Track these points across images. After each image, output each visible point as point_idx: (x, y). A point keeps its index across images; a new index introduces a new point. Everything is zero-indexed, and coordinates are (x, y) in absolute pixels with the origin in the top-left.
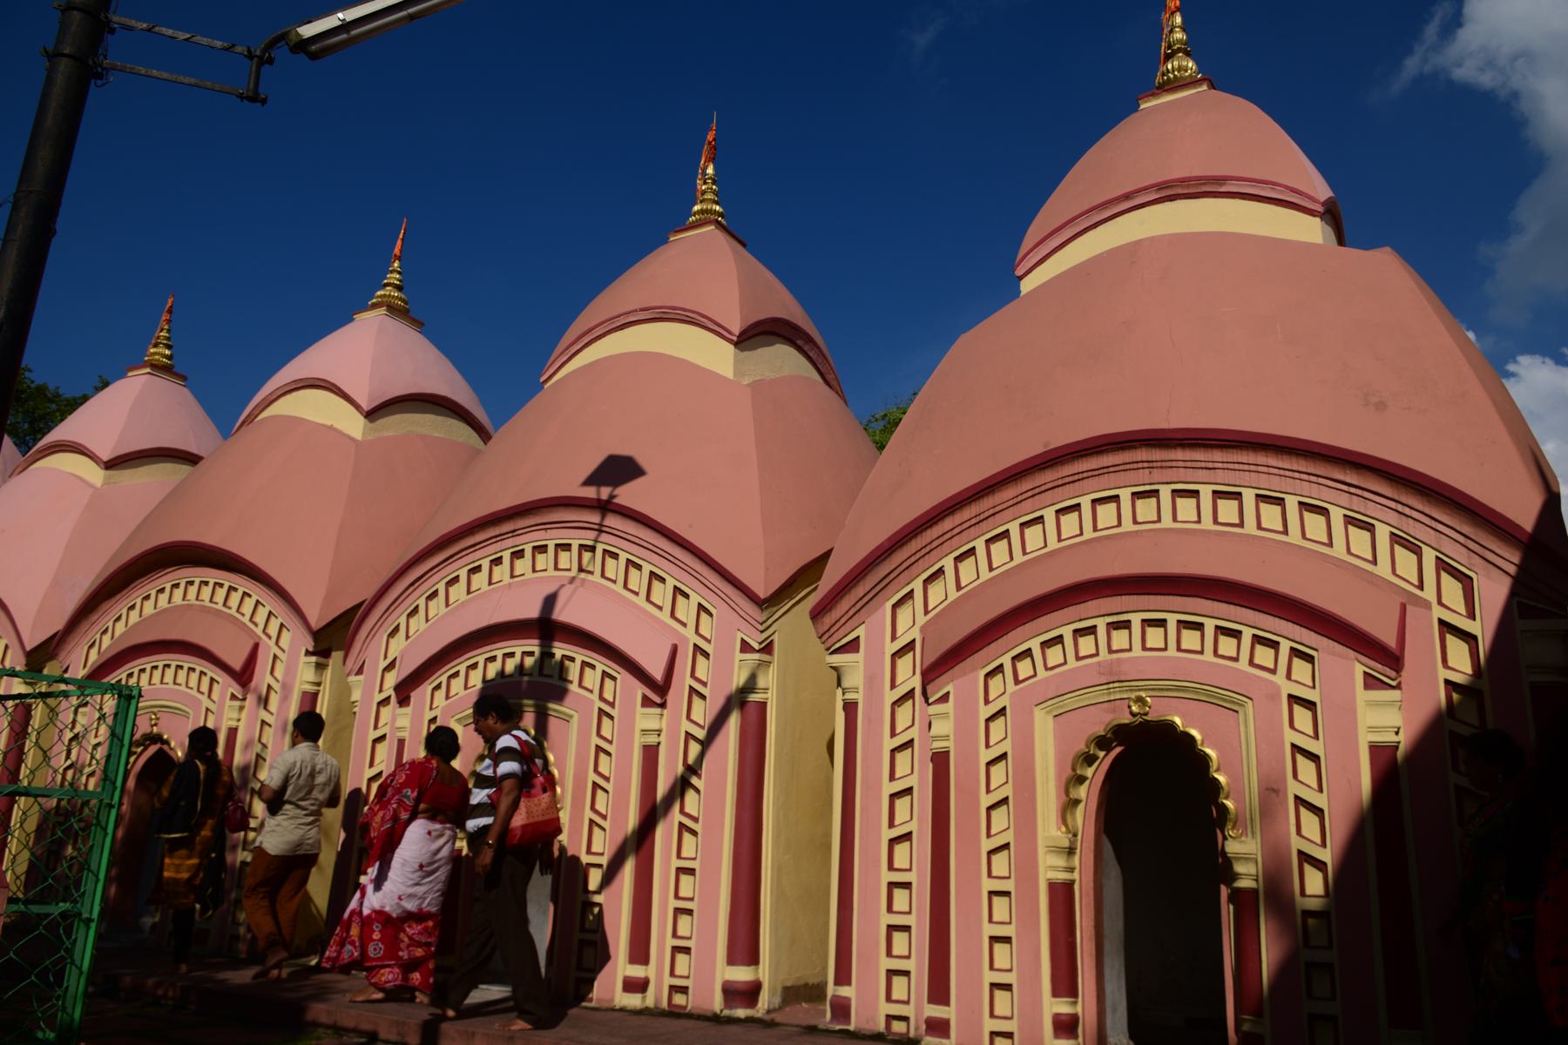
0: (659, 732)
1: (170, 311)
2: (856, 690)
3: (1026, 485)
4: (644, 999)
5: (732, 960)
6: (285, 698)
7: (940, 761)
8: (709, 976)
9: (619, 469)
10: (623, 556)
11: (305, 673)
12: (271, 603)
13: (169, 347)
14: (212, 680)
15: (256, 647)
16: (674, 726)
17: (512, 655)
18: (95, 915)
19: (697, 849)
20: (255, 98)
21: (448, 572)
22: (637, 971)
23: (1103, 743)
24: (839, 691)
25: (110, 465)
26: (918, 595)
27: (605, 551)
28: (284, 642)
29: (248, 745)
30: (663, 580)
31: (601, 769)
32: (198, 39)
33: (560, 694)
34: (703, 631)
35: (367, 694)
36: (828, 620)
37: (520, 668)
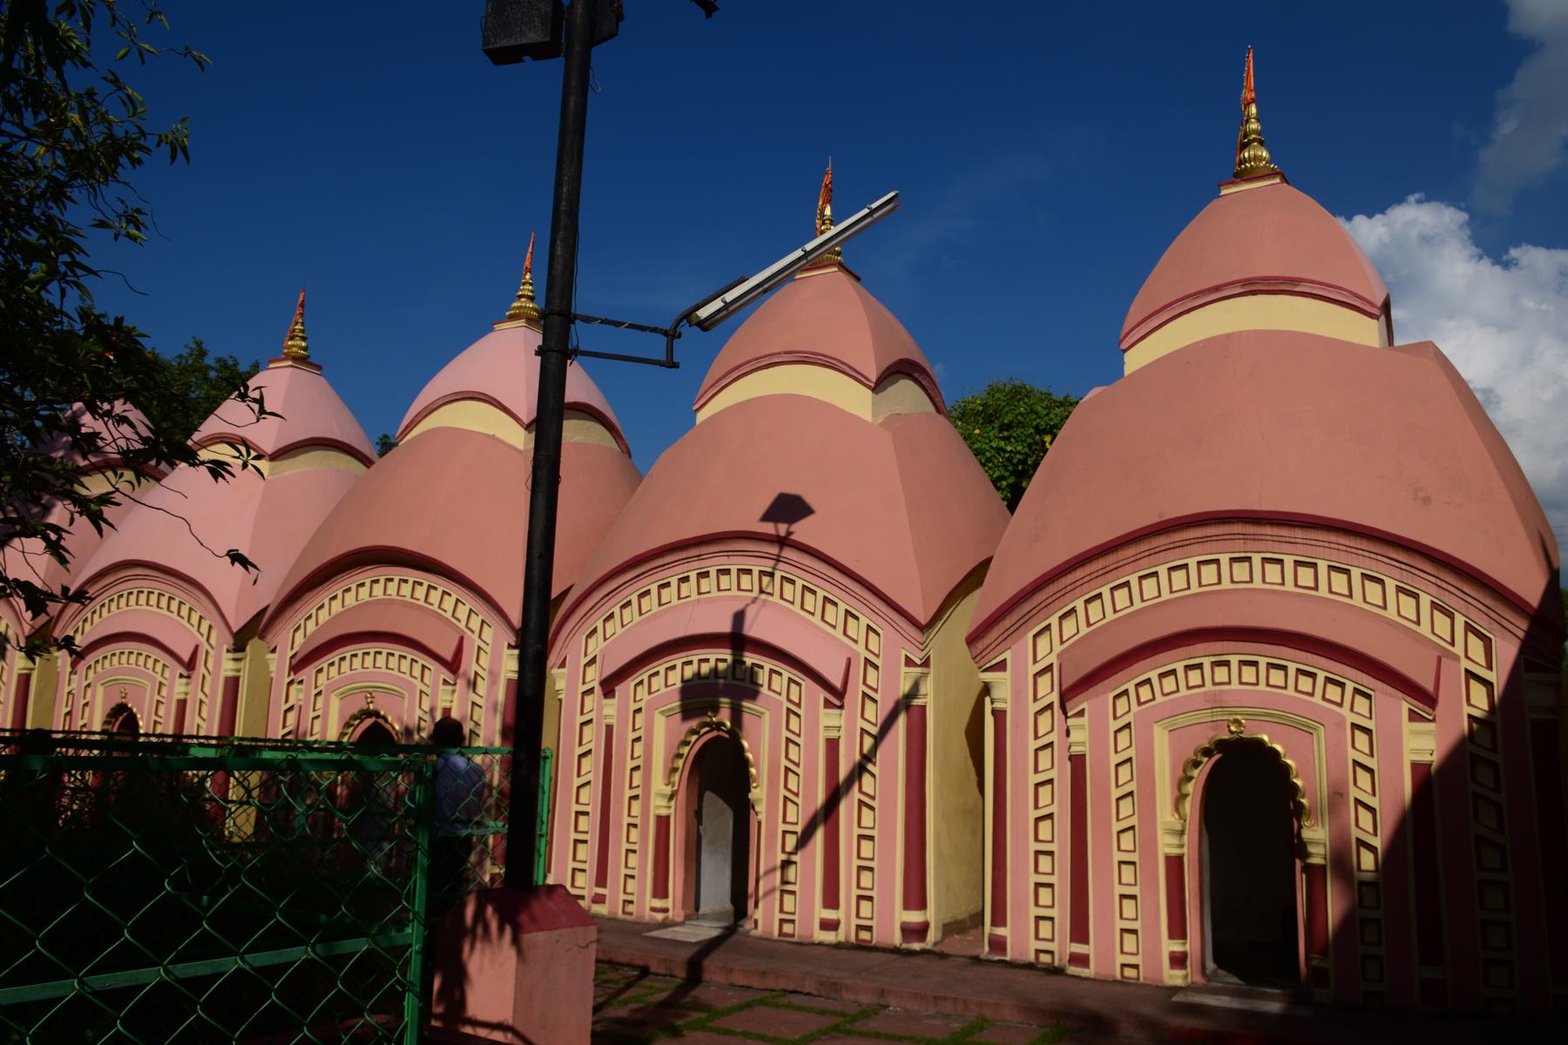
1: (302, 305)
5: (907, 907)
7: (609, 728)
8: (890, 920)
13: (304, 339)
14: (423, 667)
15: (461, 639)
16: (851, 723)
19: (874, 823)
21: (641, 586)
22: (830, 914)
26: (600, 630)
33: (753, 694)
35: (571, 685)
36: (981, 645)
37: (715, 670)
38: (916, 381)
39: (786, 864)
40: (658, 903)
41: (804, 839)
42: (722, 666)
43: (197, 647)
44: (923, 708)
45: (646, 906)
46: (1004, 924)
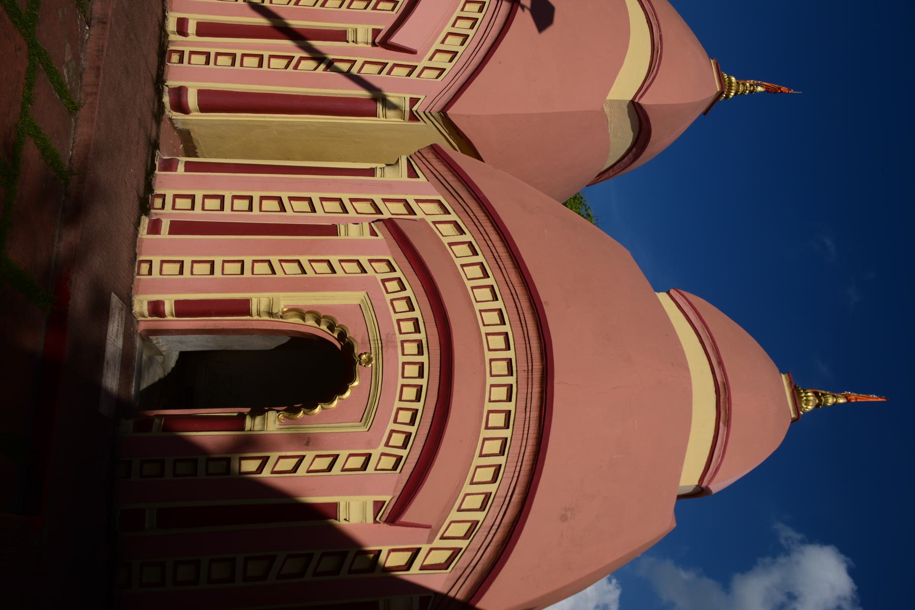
0: (355, 42)
2: (383, 175)
3: (520, 290)
4: (173, 33)
7: (332, 230)
8: (190, 77)
16: (360, 53)
22: (192, 28)
23: (342, 336)
24: (383, 165)
30: (462, 44)
34: (426, 72)
36: (430, 156)
44: (374, 114)
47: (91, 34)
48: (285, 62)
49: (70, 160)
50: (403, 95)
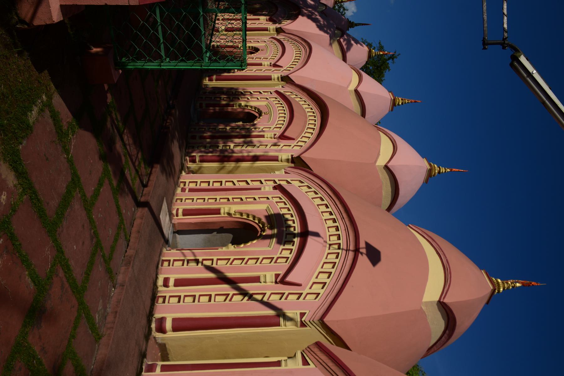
0: (265, 282)
1: (415, 102)
2: (286, 365)
4: (161, 286)
5: (174, 320)
6: (276, 151)
7: (260, 189)
8: (168, 312)
9: (374, 256)
10: (337, 261)
11: (284, 156)
12: (309, 142)
13: (402, 104)
14: (281, 128)
15: (294, 139)
16: (268, 288)
17: (294, 223)
18: (162, 67)
19: (219, 302)
20: (485, 44)
21: (325, 197)
22: (171, 282)
24: (286, 358)
25: (356, 91)
27: (338, 253)
28: (295, 148)
29: (260, 142)
30: (329, 277)
31: (250, 261)
32: (505, 18)
33: (279, 242)
34: (308, 296)
35: (277, 176)
36: (316, 350)
37: (290, 226)
38: (444, 332)
39: (197, 261)
40: (180, 212)
41: (210, 269)
42: (292, 229)
43: (282, 67)
44: (278, 325)
45: (179, 207)
46: (162, 370)
47: (114, 293)
48: (224, 297)
49: (91, 371)
50: (295, 311)
